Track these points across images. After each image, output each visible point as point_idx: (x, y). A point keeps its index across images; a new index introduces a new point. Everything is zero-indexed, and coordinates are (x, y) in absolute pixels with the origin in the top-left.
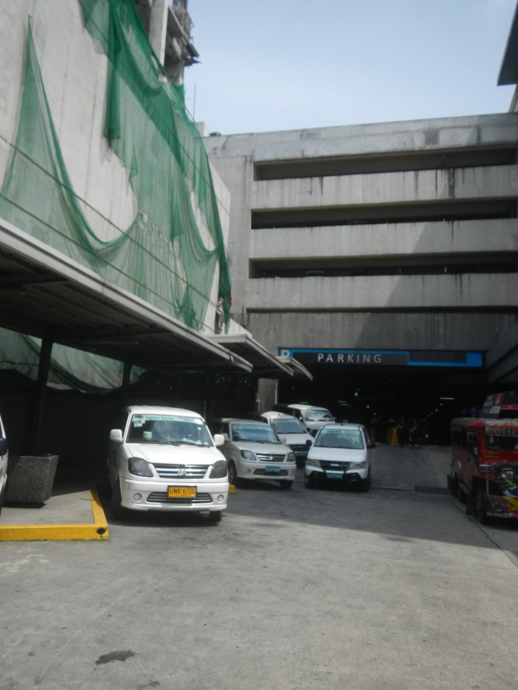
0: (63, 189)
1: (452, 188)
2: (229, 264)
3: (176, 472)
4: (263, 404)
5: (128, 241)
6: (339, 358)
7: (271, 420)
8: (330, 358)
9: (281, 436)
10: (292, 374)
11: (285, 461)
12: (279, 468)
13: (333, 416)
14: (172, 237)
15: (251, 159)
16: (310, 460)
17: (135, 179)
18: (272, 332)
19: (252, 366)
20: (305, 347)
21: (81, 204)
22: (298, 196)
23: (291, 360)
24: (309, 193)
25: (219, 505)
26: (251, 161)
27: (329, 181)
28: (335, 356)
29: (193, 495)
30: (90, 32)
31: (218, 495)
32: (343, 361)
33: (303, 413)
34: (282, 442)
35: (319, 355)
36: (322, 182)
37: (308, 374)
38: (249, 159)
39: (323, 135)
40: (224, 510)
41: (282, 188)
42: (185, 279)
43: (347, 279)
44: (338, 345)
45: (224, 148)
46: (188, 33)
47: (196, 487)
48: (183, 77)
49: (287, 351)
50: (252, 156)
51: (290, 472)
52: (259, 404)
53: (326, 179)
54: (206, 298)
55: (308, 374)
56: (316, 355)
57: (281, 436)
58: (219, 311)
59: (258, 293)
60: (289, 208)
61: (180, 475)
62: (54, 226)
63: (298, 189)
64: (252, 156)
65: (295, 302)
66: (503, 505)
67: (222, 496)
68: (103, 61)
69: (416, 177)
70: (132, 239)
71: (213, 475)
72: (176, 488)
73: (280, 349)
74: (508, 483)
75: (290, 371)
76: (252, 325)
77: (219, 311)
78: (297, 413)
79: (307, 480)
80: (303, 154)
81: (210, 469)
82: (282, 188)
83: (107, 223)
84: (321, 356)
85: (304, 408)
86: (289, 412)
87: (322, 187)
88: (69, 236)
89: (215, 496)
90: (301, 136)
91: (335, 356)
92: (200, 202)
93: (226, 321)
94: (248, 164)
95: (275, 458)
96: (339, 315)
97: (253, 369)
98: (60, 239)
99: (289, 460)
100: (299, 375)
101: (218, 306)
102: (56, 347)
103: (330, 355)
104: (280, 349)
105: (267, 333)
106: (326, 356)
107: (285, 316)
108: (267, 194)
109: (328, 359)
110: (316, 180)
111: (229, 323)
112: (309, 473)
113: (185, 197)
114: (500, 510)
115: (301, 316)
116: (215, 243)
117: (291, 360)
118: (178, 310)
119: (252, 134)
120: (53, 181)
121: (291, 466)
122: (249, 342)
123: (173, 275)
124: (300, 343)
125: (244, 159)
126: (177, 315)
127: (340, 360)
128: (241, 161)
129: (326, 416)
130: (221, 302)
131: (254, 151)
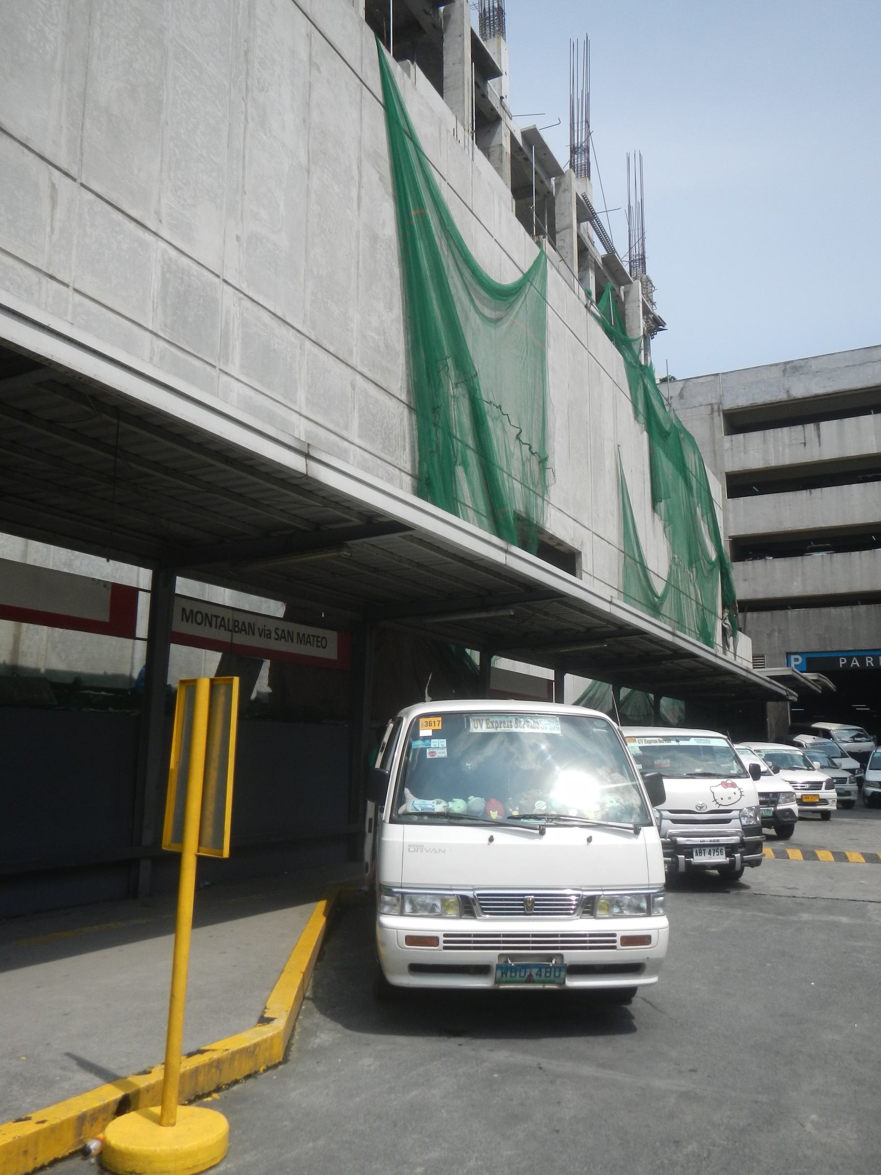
0: (638, 565)
2: (731, 569)
3: (804, 786)
4: (773, 724)
5: (672, 589)
6: (867, 661)
7: (807, 745)
8: (855, 663)
9: (836, 761)
10: (820, 692)
11: (847, 784)
12: (843, 789)
13: (870, 734)
14: (690, 564)
15: (719, 408)
16: (869, 782)
17: (667, 530)
18: (776, 634)
19: (797, 695)
20: (822, 650)
21: (652, 576)
22: (787, 450)
23: (819, 676)
24: (803, 444)
25: (832, 807)
26: (719, 411)
27: (828, 427)
28: (862, 660)
29: (818, 800)
30: (638, 421)
31: (832, 800)
32: (872, 665)
33: (833, 733)
34: (839, 766)
35: (841, 659)
36: (818, 429)
37: (831, 685)
38: (716, 407)
39: (814, 366)
40: (833, 811)
41: (765, 441)
42: (701, 603)
43: (865, 553)
44: (864, 645)
45: (681, 396)
46: (651, 302)
47: (818, 795)
48: (650, 353)
49: (798, 657)
50: (720, 403)
51: (853, 793)
52: (769, 724)
53: (824, 425)
54: (716, 614)
55: (831, 685)
56: (837, 659)
57: (836, 761)
58: (726, 624)
59: (745, 580)
60: (776, 466)
61: (807, 788)
62: (637, 599)
63: (787, 441)
64: (720, 403)
65: (797, 589)
67: (834, 801)
68: (645, 434)
70: (672, 585)
71: (827, 788)
72: (807, 796)
73: (788, 654)
75: (818, 688)
76: (749, 627)
77: (726, 624)
78: (826, 734)
79: (866, 801)
80: (789, 396)
81: (824, 784)
82: (765, 441)
83: (657, 577)
84: (843, 661)
85: (832, 727)
86: (815, 732)
87: (819, 436)
88: (643, 602)
89: (830, 801)
90: (784, 371)
91: (862, 660)
92: (702, 516)
93: (734, 635)
94: (716, 414)
95: (838, 781)
96: (862, 609)
97: (799, 698)
98: (639, 605)
99: (851, 782)
100: (825, 687)
101: (723, 619)
103: (854, 658)
104: (788, 654)
105: (770, 636)
106: (850, 659)
107: (793, 613)
108: (746, 452)
109: (853, 663)
110: (810, 427)
111: (737, 636)
112: (869, 794)
113: (693, 516)
115: (812, 613)
116: (716, 550)
117: (819, 676)
118: (698, 635)
119: (717, 374)
120: (633, 561)
121: (854, 787)
122: (795, 674)
123: (694, 603)
124: (815, 646)
125: (709, 407)
126: (698, 640)
127: (869, 663)
128: (705, 411)
129: (858, 736)
130: (726, 614)
131: (722, 396)
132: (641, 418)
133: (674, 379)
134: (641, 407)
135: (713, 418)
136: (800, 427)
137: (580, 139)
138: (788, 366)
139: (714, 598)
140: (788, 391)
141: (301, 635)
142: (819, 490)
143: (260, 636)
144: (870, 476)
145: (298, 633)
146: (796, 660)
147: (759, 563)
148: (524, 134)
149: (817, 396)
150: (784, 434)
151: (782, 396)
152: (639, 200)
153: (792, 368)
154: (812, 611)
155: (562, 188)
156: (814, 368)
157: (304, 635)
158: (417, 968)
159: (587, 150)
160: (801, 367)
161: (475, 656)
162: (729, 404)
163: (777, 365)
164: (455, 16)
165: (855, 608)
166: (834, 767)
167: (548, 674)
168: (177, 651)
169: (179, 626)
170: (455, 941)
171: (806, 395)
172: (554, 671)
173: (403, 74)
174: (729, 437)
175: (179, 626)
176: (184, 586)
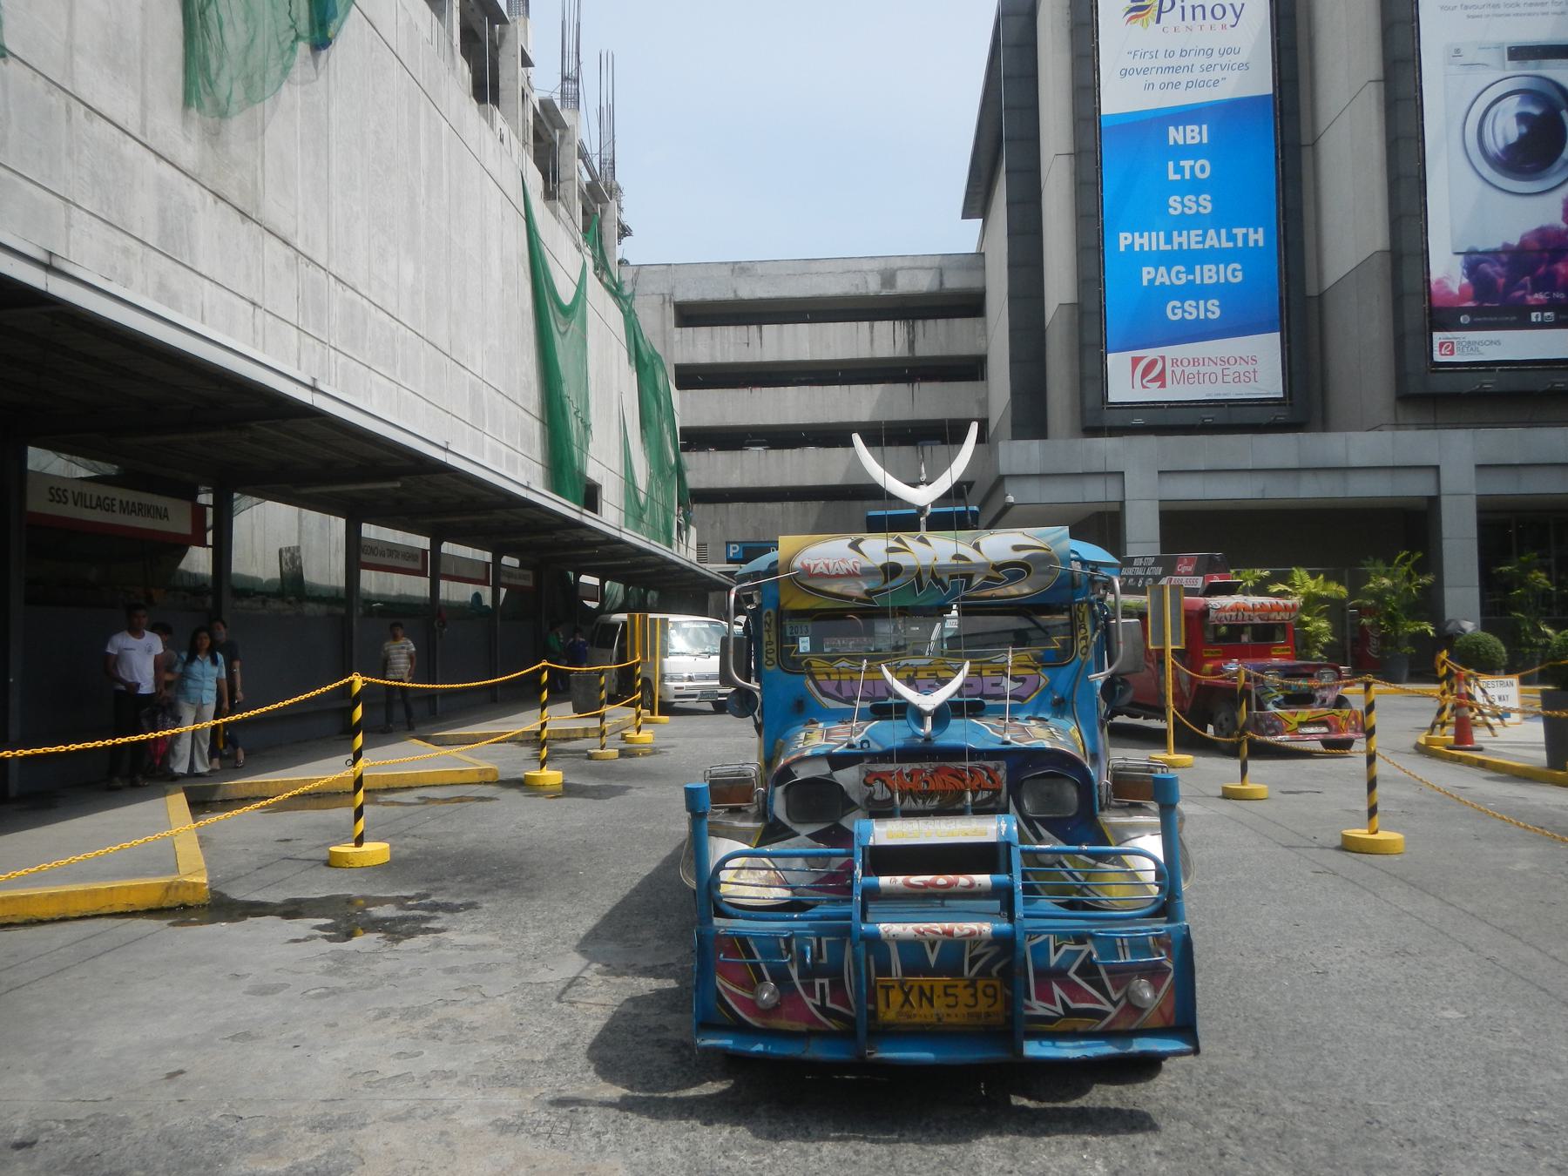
1: (911, 344)
14: (659, 474)
15: (670, 299)
18: (718, 525)
22: (732, 349)
27: (769, 330)
38: (667, 298)
39: (760, 269)
41: (712, 338)
63: (732, 340)
66: (1277, 723)
69: (872, 328)
74: (1272, 692)
80: (736, 295)
82: (712, 338)
87: (761, 338)
90: (733, 271)
94: (667, 305)
102: (607, 584)
104: (728, 543)
105: (713, 526)
107: (733, 507)
110: (754, 328)
114: (1273, 731)
128: (657, 300)
130: (681, 512)
131: (674, 287)
132: (633, 363)
133: (627, 262)
134: (633, 354)
135: (664, 309)
136: (745, 327)
137: (571, 68)
138: (737, 267)
139: (673, 501)
140: (735, 292)
141: (124, 503)
142: (758, 389)
143: (76, 504)
144: (803, 379)
145: (121, 501)
146: (734, 548)
147: (702, 455)
148: (541, 102)
149: (761, 299)
150: (730, 332)
151: (730, 296)
152: (610, 102)
153: (740, 269)
154: (750, 506)
155: (566, 141)
156: (759, 271)
157: (128, 503)
158: (677, 697)
159: (577, 81)
160: (748, 269)
161: (571, 574)
162: (680, 296)
163: (726, 263)
164: (509, 36)
165: (785, 504)
166: (62, 950)
167: (423, 542)
168: (443, 584)
169: (365, 558)
170: (689, 688)
171: (752, 297)
172: (428, 539)
173: (882, 746)
174: (679, 329)
175: (365, 558)
176: (369, 531)
